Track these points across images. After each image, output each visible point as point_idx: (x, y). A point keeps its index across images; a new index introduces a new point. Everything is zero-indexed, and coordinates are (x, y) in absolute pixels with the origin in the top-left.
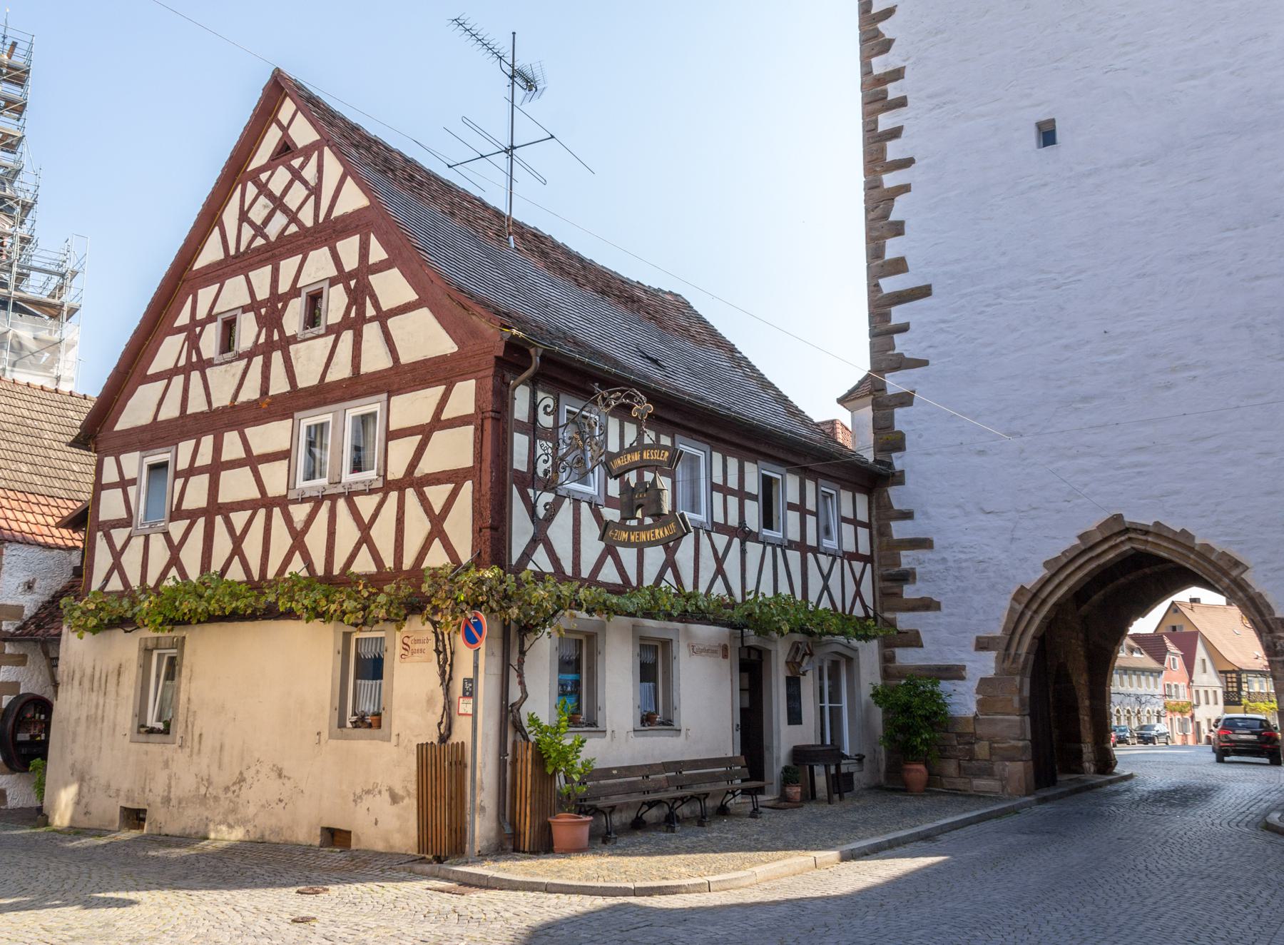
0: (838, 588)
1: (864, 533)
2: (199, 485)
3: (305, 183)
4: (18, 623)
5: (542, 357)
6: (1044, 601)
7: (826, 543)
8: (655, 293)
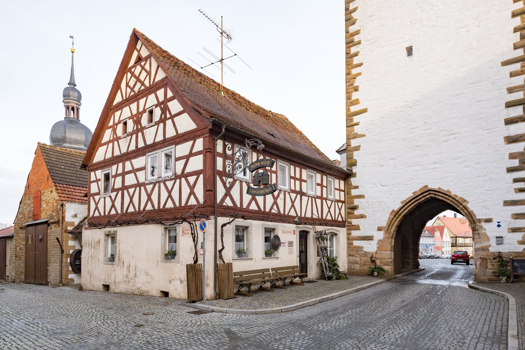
0: (337, 212)
1: (342, 194)
2: (119, 179)
3: (146, 71)
4: (73, 227)
5: (226, 129)
6: (400, 214)
7: (330, 197)
8: (275, 115)
